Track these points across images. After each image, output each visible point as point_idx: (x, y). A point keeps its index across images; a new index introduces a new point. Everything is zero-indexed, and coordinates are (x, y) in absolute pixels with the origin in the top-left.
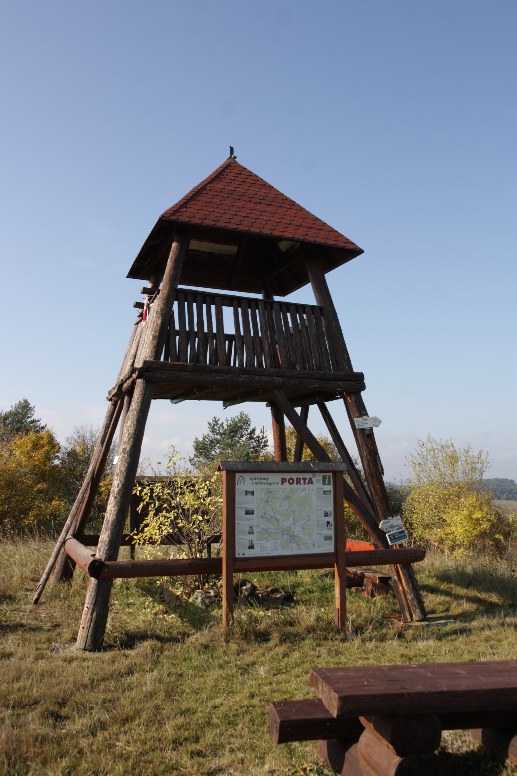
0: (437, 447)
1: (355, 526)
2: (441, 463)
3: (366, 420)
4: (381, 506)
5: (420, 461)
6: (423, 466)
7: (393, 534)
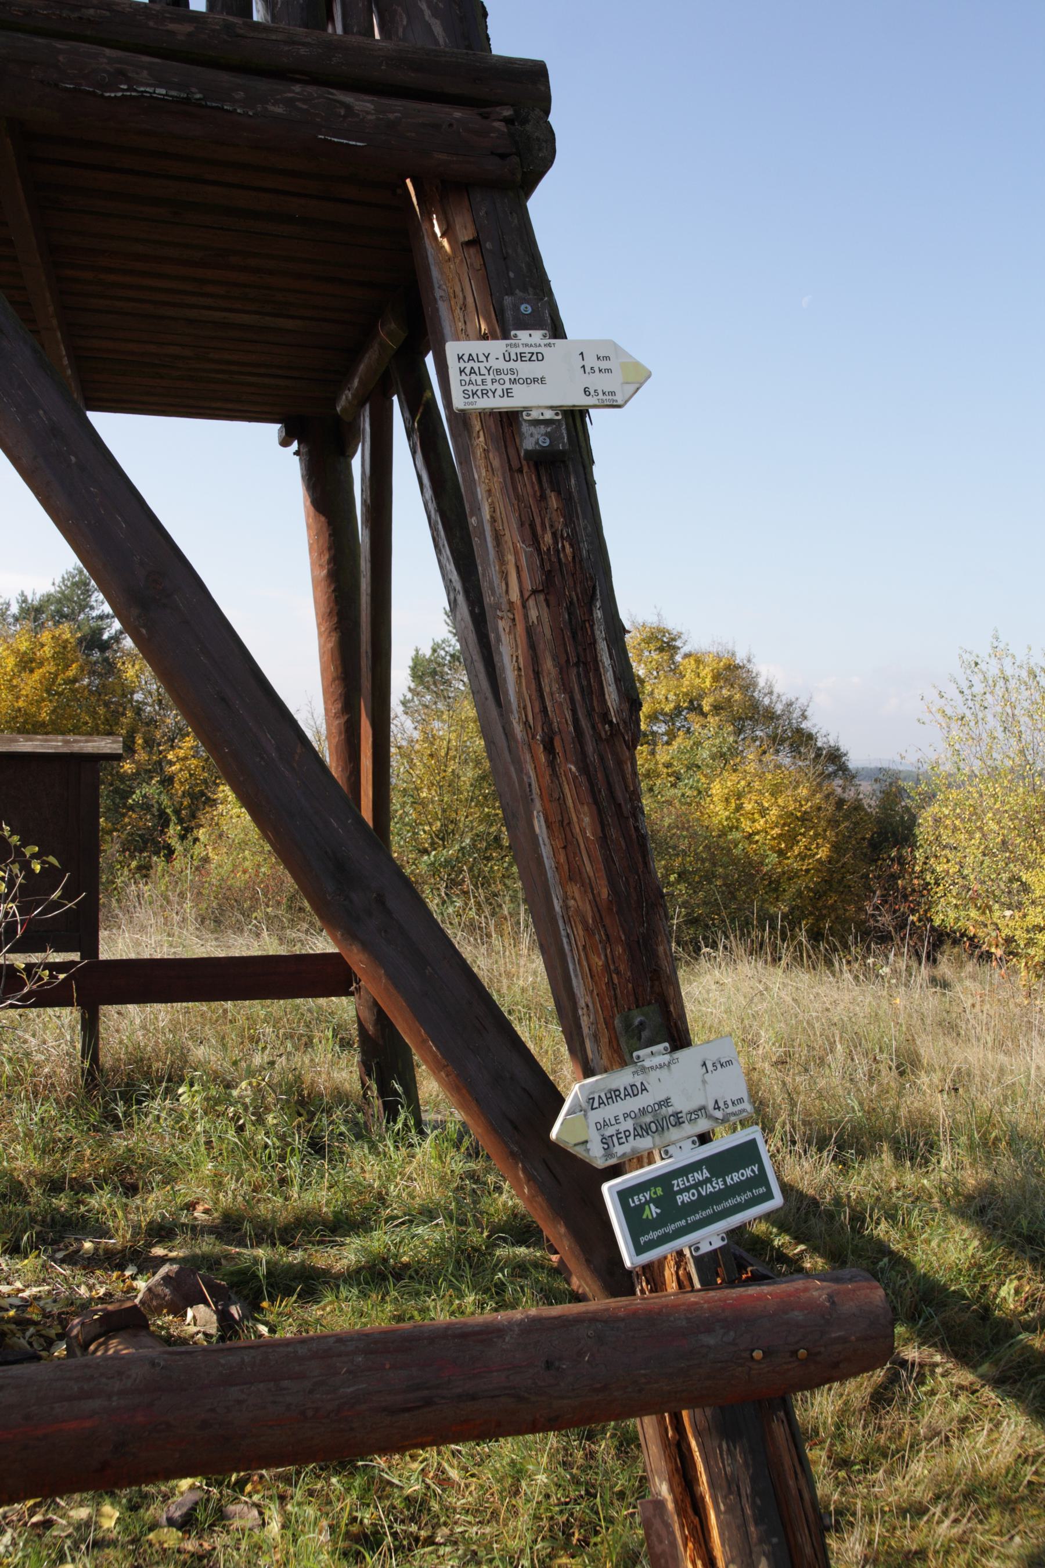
0: (1017, 672)
1: (778, 882)
2: (1024, 719)
3: (539, 357)
4: (598, 962)
5: (962, 710)
6: (972, 724)
7: (664, 1180)
